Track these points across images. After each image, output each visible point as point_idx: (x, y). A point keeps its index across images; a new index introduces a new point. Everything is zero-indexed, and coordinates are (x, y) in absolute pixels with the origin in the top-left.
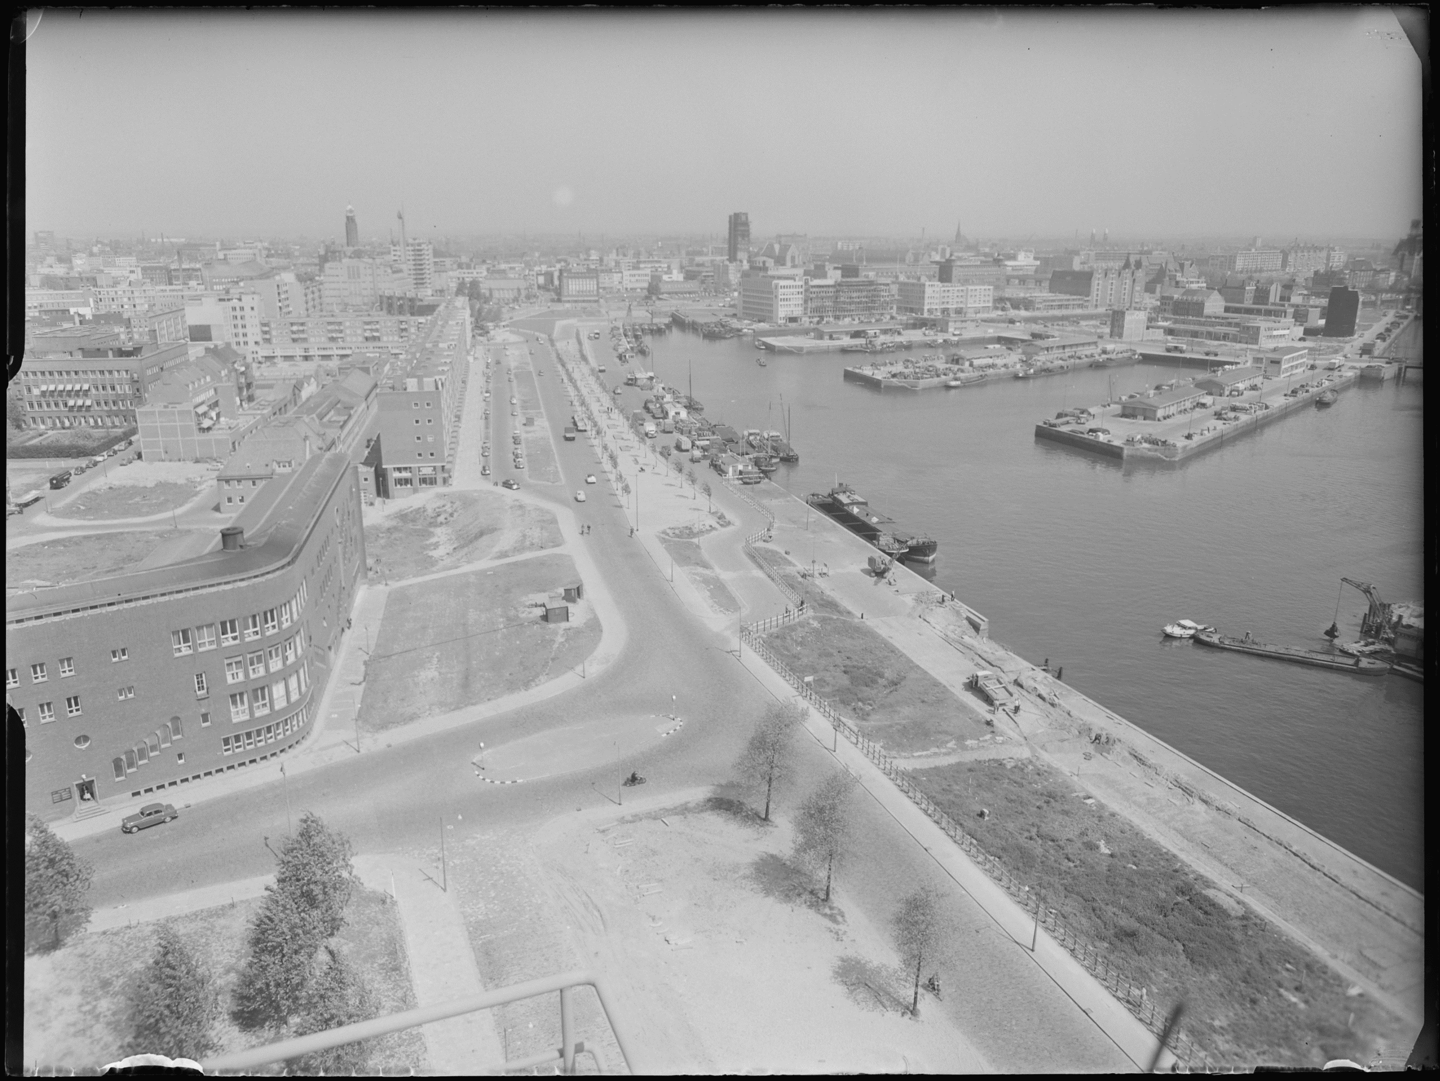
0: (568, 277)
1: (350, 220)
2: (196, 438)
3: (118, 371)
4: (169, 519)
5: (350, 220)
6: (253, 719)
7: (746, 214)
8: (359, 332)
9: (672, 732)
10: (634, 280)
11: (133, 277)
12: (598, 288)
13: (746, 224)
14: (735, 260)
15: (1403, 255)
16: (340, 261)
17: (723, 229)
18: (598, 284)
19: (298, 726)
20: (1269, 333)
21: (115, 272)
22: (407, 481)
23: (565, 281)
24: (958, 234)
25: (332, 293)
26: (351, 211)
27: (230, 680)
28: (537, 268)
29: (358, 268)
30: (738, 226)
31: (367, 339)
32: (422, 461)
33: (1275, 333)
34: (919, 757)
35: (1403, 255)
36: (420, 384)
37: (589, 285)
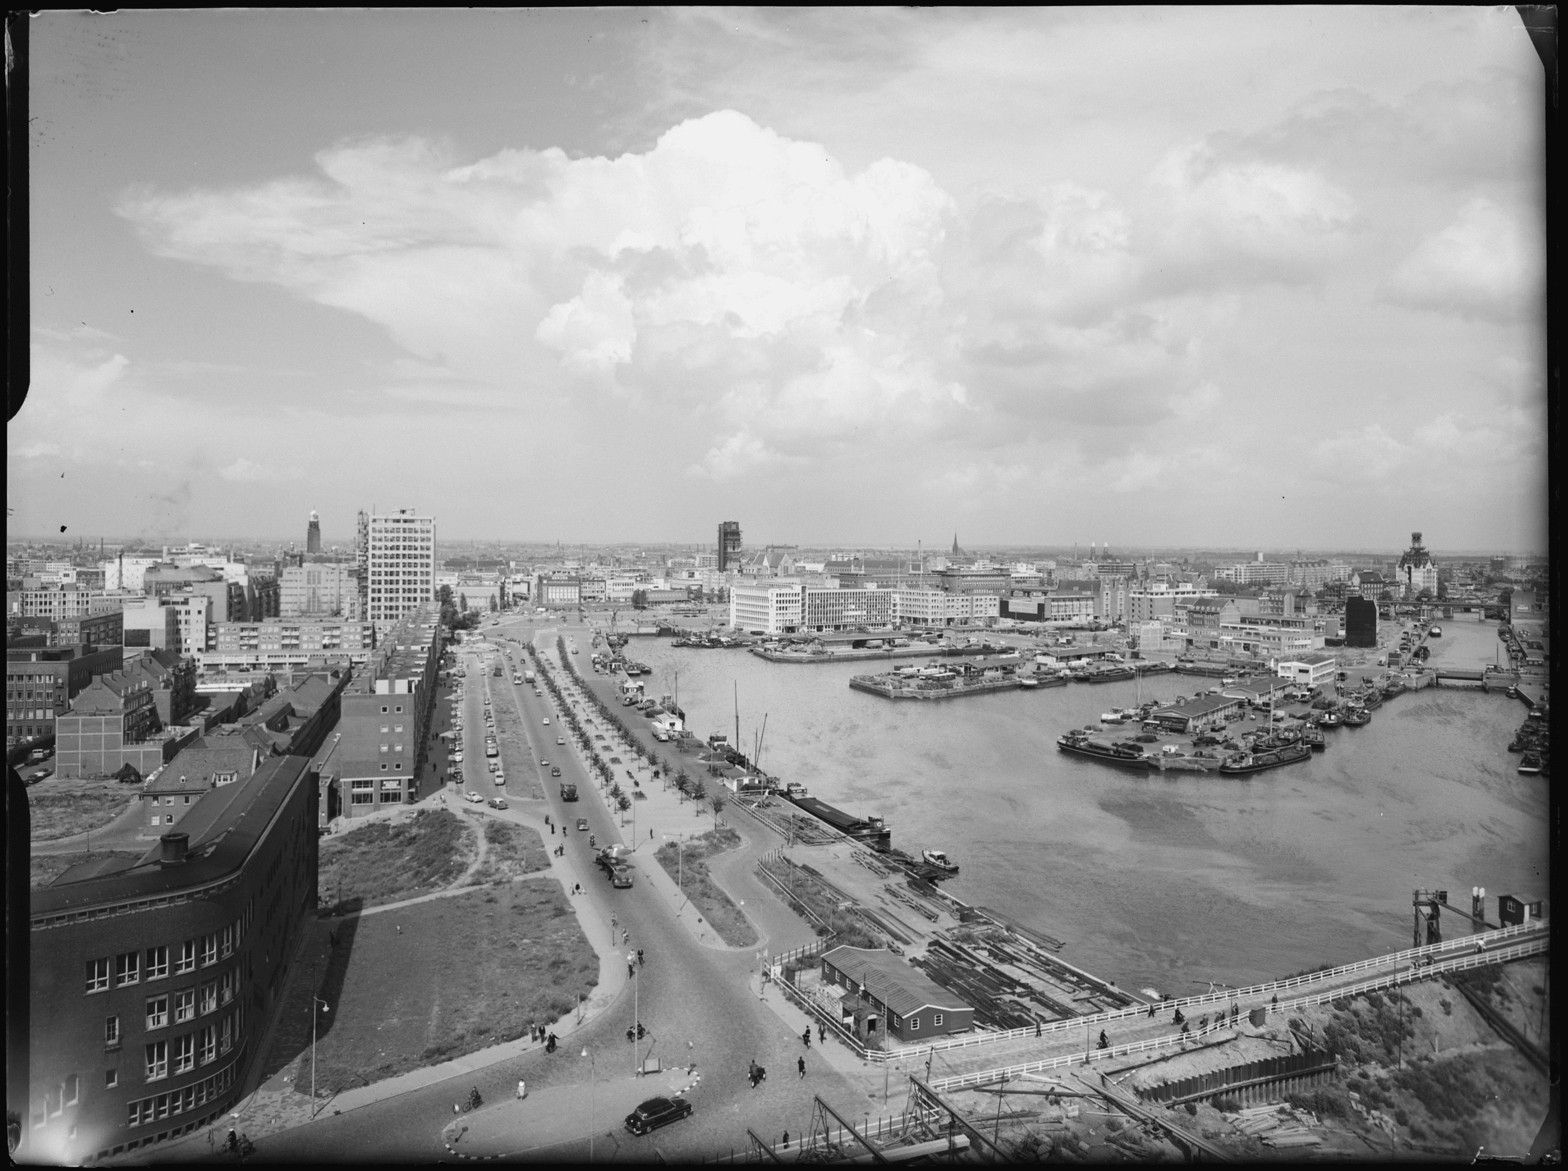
0: (548, 585)
1: (314, 526)
2: (122, 750)
3: (40, 676)
4: (83, 842)
5: (314, 526)
6: (172, 1079)
7: (736, 524)
8: (317, 638)
9: (687, 1089)
10: (619, 588)
11: (66, 581)
12: (580, 597)
13: (737, 533)
14: (725, 570)
15: (1409, 568)
16: (301, 566)
17: (712, 539)
18: (580, 592)
19: (226, 1088)
20: (1290, 643)
21: (45, 578)
22: (367, 798)
23: (544, 589)
24: (955, 547)
25: (290, 599)
26: (316, 517)
27: (151, 1026)
28: (513, 577)
29: (320, 573)
30: (730, 533)
31: (325, 647)
32: (387, 774)
33: (1297, 643)
34: (1079, 657)
35: (1409, 568)
36: (392, 687)
37: (571, 594)
